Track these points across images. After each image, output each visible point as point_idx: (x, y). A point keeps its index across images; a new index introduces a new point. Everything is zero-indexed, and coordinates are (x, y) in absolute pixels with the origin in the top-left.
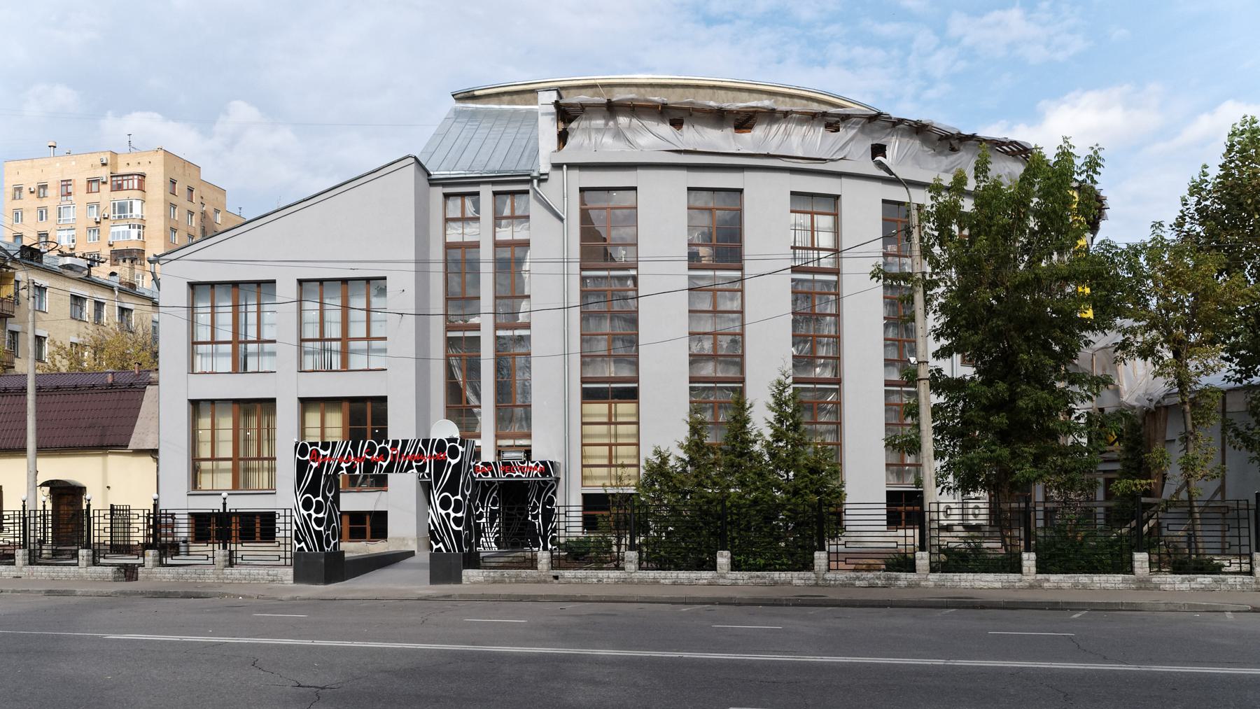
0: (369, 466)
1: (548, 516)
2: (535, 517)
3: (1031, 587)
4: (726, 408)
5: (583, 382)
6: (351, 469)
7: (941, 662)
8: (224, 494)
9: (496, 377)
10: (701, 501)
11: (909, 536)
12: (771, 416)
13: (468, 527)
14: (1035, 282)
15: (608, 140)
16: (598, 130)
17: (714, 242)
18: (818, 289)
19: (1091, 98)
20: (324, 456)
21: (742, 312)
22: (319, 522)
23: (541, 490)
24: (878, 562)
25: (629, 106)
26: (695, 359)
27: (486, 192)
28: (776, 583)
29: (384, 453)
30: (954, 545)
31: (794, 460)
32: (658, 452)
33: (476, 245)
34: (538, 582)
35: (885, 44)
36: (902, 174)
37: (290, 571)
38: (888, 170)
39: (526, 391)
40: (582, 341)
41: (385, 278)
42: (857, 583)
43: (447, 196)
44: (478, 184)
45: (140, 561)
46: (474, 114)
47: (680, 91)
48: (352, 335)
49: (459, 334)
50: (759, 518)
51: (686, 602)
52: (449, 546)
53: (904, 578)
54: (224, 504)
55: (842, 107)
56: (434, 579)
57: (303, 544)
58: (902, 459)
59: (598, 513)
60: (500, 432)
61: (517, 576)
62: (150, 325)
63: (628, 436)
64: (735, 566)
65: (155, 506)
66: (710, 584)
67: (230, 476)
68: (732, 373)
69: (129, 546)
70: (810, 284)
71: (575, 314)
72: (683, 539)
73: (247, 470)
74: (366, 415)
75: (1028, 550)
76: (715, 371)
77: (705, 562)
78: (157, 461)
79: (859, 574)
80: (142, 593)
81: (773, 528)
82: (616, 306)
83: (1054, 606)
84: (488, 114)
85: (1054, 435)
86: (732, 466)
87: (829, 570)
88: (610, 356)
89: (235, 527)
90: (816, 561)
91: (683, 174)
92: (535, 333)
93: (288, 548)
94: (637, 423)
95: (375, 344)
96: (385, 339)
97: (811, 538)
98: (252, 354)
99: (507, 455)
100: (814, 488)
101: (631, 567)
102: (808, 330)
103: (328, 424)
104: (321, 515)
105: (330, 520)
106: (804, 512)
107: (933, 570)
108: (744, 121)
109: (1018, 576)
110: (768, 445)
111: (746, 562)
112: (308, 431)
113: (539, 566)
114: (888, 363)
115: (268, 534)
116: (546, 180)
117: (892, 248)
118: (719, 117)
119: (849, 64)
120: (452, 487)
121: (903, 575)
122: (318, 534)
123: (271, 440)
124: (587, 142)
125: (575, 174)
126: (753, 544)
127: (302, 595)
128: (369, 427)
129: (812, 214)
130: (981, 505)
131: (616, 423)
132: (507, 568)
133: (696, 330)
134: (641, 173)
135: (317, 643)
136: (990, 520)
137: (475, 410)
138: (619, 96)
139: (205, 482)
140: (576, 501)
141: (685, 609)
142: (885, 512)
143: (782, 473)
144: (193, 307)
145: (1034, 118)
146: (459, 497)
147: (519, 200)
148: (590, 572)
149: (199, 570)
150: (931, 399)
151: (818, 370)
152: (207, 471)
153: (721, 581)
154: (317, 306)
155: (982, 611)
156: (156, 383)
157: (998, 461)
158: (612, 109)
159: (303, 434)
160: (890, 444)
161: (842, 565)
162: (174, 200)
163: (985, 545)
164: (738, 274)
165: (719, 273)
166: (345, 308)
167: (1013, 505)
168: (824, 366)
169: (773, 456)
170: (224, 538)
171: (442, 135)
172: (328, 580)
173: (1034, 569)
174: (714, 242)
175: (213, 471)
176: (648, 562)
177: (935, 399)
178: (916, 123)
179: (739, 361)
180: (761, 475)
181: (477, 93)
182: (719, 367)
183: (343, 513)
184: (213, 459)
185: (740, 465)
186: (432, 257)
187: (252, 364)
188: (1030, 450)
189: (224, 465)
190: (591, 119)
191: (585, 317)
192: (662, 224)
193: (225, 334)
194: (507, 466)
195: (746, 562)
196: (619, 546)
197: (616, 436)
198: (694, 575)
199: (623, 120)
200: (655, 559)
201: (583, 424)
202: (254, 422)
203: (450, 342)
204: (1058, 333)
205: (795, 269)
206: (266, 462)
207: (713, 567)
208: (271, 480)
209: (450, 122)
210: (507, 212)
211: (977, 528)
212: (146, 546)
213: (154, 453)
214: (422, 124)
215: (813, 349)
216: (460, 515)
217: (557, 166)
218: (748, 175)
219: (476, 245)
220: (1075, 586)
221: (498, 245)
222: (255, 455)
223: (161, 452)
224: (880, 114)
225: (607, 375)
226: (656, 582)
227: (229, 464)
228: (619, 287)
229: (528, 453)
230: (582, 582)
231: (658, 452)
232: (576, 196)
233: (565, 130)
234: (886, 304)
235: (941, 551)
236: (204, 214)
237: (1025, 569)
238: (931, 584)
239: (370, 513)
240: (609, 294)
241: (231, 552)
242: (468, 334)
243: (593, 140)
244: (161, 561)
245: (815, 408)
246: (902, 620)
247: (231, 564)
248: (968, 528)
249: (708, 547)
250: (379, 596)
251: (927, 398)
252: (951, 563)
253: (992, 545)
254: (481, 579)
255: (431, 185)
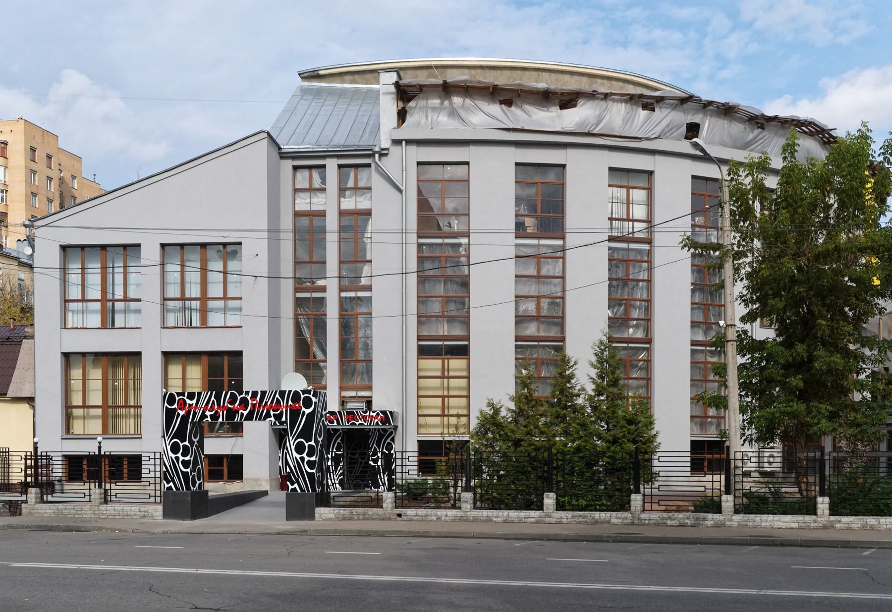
0: (231, 414)
1: (389, 459)
2: (376, 461)
3: (825, 527)
4: (547, 365)
5: (419, 340)
6: (215, 417)
7: (754, 592)
8: (100, 439)
9: (341, 335)
10: (529, 449)
11: (716, 481)
12: (594, 373)
13: (320, 470)
14: (834, 253)
15: (443, 118)
16: (434, 109)
17: (539, 212)
18: (632, 257)
19: (869, 75)
20: (190, 405)
21: (563, 277)
22: (186, 464)
23: (381, 437)
24: (686, 504)
25: (462, 87)
26: (520, 320)
27: (332, 165)
28: (596, 522)
29: (244, 402)
30: (754, 490)
31: (614, 412)
32: (491, 405)
33: (322, 214)
34: (384, 519)
35: (682, 26)
36: (714, 151)
37: (160, 508)
38: (702, 150)
39: (368, 348)
40: (418, 302)
41: (240, 243)
42: (669, 522)
43: (296, 168)
44: (324, 157)
45: (24, 498)
46: (319, 92)
47: (507, 73)
48: (210, 295)
49: (307, 295)
50: (582, 464)
51: (518, 538)
52: (179, 485)
53: (712, 518)
54: (100, 448)
55: (657, 90)
56: (290, 516)
57: (171, 484)
58: (705, 412)
59: (437, 458)
60: (344, 385)
61: (364, 514)
62: (16, 283)
63: (459, 389)
64: (560, 507)
65: (36, 449)
66: (537, 522)
67: (100, 422)
68: (554, 332)
69: (9, 484)
70: (625, 253)
71: (413, 279)
72: (514, 483)
73: (115, 417)
74: (224, 368)
75: (822, 494)
76: (539, 331)
77: (532, 503)
78: (33, 408)
79: (670, 514)
80: (27, 527)
81: (594, 473)
82: (449, 272)
83: (846, 545)
84: (331, 92)
85: (846, 391)
86: (558, 417)
87: (644, 510)
88: (443, 316)
89: (105, 468)
90: (632, 503)
91: (512, 150)
92: (375, 294)
93: (158, 487)
94: (468, 377)
95: (231, 304)
96: (240, 299)
97: (628, 482)
98: (120, 311)
99: (350, 405)
100: (631, 437)
101: (467, 506)
102: (622, 294)
103: (188, 376)
104: (188, 458)
105: (196, 463)
106: (622, 459)
107: (737, 512)
108: (568, 100)
109: (813, 517)
110: (590, 399)
111: (569, 503)
112: (170, 382)
113: (384, 505)
114: (694, 324)
115: (135, 475)
116: (386, 155)
117: (699, 220)
118: (545, 98)
119: (649, 46)
120: (306, 433)
121: (710, 516)
122: (185, 475)
123: (137, 389)
124: (423, 120)
125: (413, 149)
126: (574, 486)
127: (172, 529)
128: (226, 378)
129: (628, 188)
130: (775, 454)
131: (449, 377)
132: (355, 506)
133: (521, 294)
134: (473, 149)
135: (200, 571)
136: (783, 467)
137: (322, 364)
138: (453, 77)
139: (78, 427)
140: (412, 447)
141: (518, 544)
142: (689, 459)
143: (603, 424)
144: (64, 269)
145: (817, 93)
146: (312, 443)
147: (363, 174)
148: (430, 511)
149: (78, 506)
150: (735, 360)
151: (631, 330)
152: (78, 418)
153: (548, 520)
154: (178, 268)
155: (781, 548)
156: (32, 337)
157: (794, 415)
158: (447, 89)
159: (166, 385)
160: (696, 400)
161: (655, 507)
162: (34, 166)
163: (784, 490)
164: (560, 242)
165: (543, 242)
166: (204, 270)
167: (811, 454)
168: (637, 327)
169: (595, 408)
170: (95, 477)
171: (290, 111)
172: (194, 516)
173: (827, 512)
174: (539, 212)
175: (84, 418)
176: (482, 502)
177: (741, 360)
178: (723, 105)
179: (560, 322)
180: (583, 425)
181: (321, 72)
182: (542, 327)
183: (206, 456)
184: (84, 406)
185: (565, 416)
186: (282, 227)
187: (119, 320)
188: (825, 408)
189: (93, 412)
190: (427, 99)
191: (422, 280)
192: (492, 193)
193: (95, 293)
194: (351, 415)
195: (569, 503)
196: (455, 486)
197: (448, 389)
198: (523, 514)
199: (457, 100)
200: (488, 499)
201: (419, 377)
202: (121, 373)
203: (299, 302)
204: (854, 300)
205: (611, 239)
206: (132, 410)
207: (540, 507)
208: (137, 426)
209: (298, 98)
210: (351, 184)
211: (771, 474)
212: (24, 487)
213: (30, 400)
214: (271, 103)
215: (627, 311)
216: (313, 459)
217: (397, 142)
218: (571, 152)
219: (322, 214)
220: (864, 527)
221: (342, 214)
222: (123, 403)
223: (37, 400)
224: (712, 102)
225: (441, 333)
226: (489, 520)
227: (99, 412)
228: (452, 254)
229: (369, 403)
230: (423, 519)
231: (491, 405)
232: (413, 168)
233: (404, 108)
234: (693, 271)
235: (744, 495)
236: (62, 180)
237: (819, 512)
238: (735, 524)
239: (227, 456)
240: (443, 259)
241: (106, 490)
242: (315, 295)
243: (432, 119)
244: (42, 498)
245: (629, 364)
246: (712, 555)
247: (106, 502)
248: (764, 474)
249: (536, 489)
250: (242, 531)
251: (734, 358)
252: (753, 505)
253: (790, 490)
254: (332, 516)
255: (282, 158)
